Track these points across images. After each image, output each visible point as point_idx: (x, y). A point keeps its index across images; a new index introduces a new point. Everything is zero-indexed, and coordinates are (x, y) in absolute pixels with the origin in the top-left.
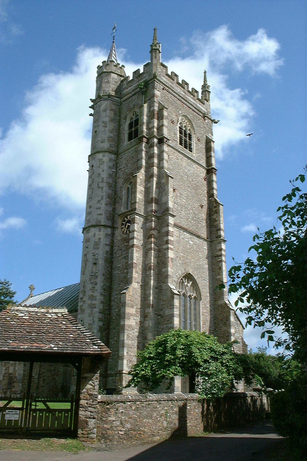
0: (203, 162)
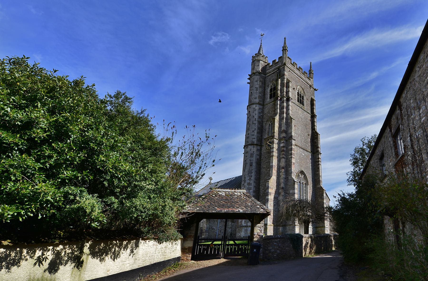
0: (309, 111)
